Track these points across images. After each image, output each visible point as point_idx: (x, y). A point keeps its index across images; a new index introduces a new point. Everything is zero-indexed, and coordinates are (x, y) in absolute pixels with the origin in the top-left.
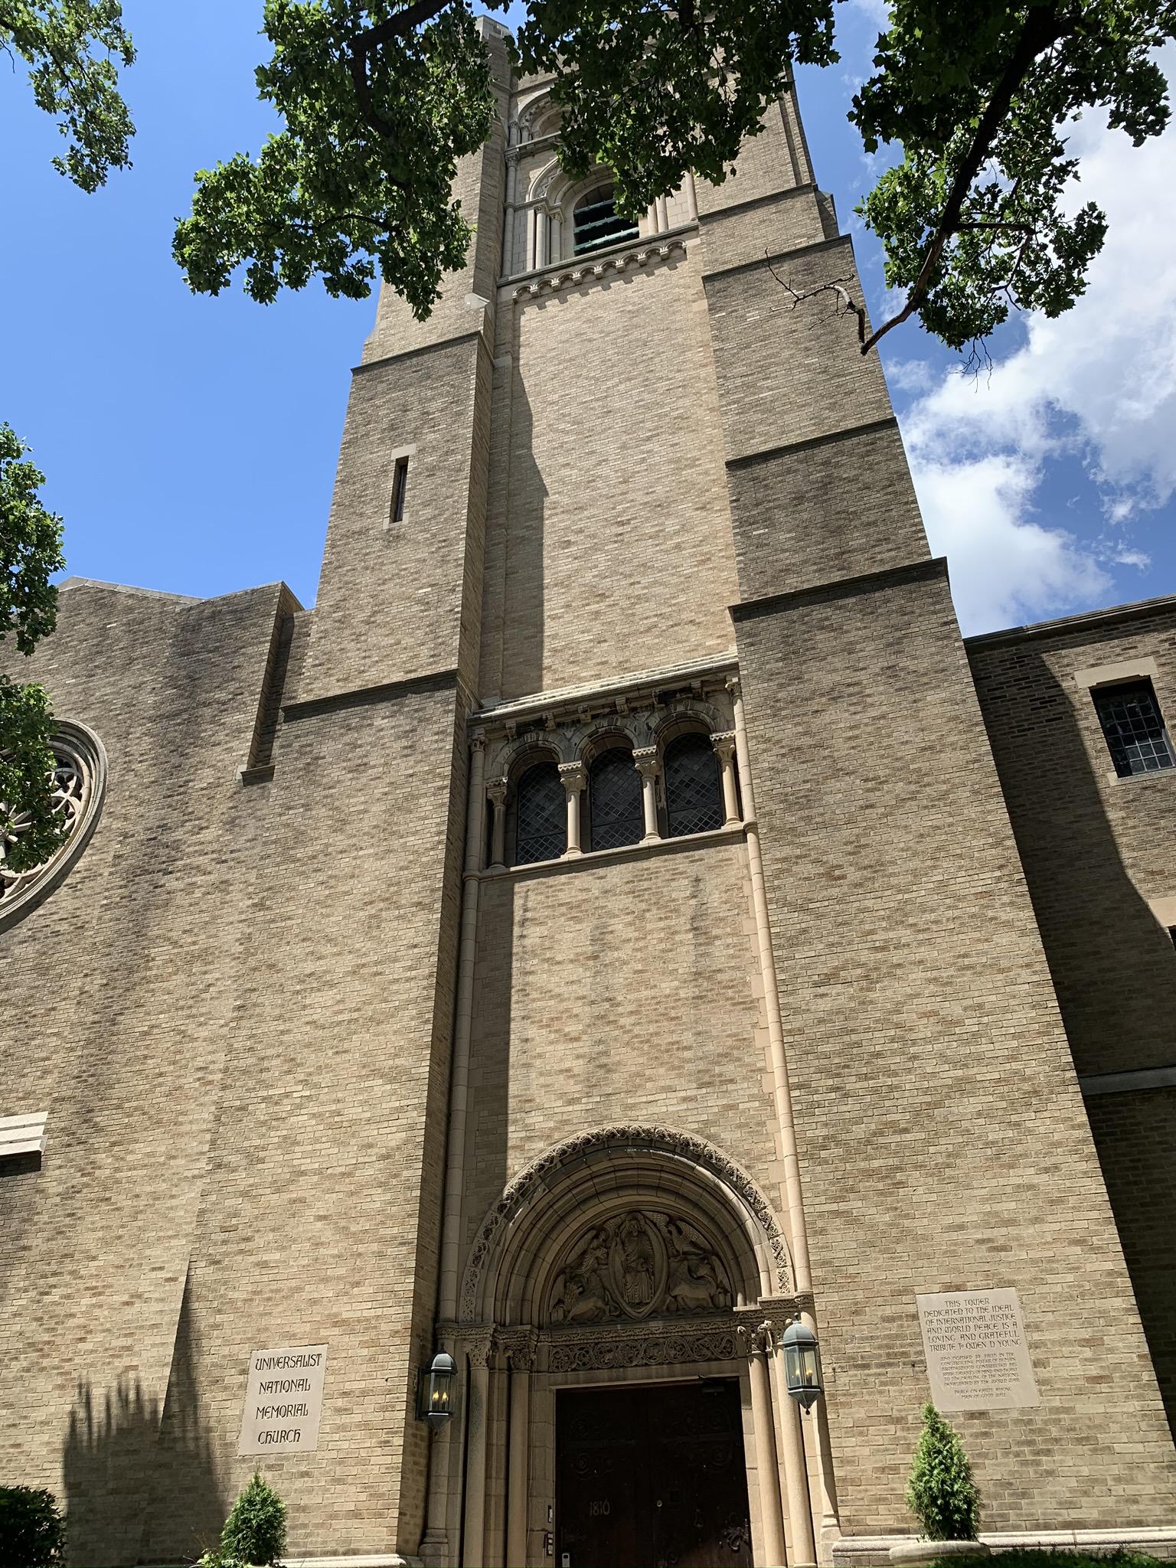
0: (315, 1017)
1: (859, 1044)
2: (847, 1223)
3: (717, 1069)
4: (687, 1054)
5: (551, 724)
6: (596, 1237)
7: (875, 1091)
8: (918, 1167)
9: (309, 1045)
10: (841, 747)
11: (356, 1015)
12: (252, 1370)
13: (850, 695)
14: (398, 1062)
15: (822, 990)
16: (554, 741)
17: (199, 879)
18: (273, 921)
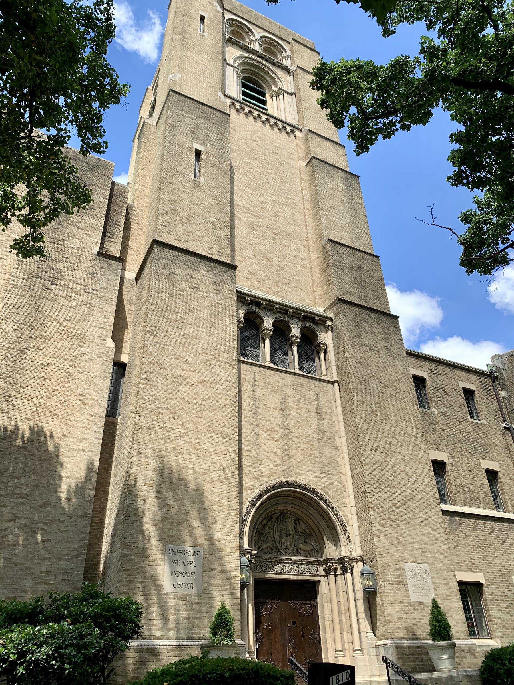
0: (184, 397)
1: (384, 475)
2: (385, 535)
3: (327, 468)
4: (317, 460)
6: (270, 520)
7: (390, 492)
8: (403, 521)
9: (183, 409)
11: (203, 402)
14: (224, 429)
15: (373, 452)
17: (74, 296)
18: (158, 343)
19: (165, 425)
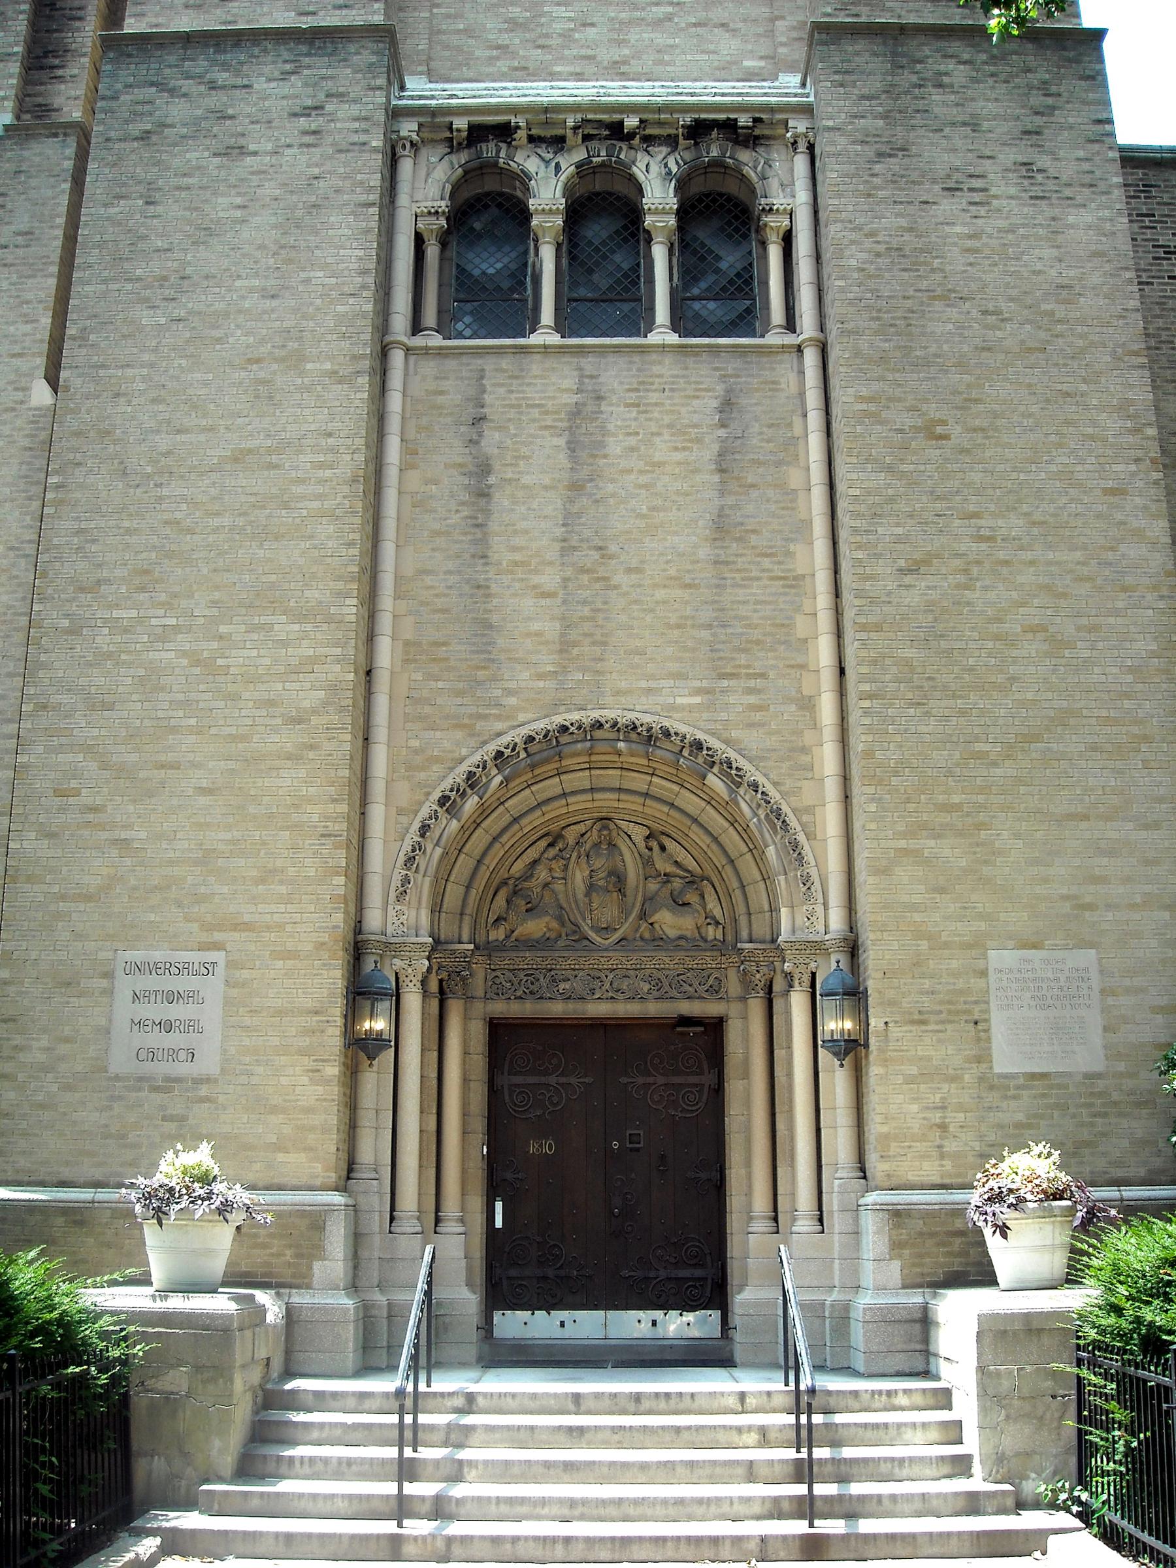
0: (178, 515)
5: (521, 135)
6: (551, 845)
10: (956, 261)
12: (119, 973)
13: (971, 190)
15: (908, 580)
16: (530, 162)
19: (116, 614)
